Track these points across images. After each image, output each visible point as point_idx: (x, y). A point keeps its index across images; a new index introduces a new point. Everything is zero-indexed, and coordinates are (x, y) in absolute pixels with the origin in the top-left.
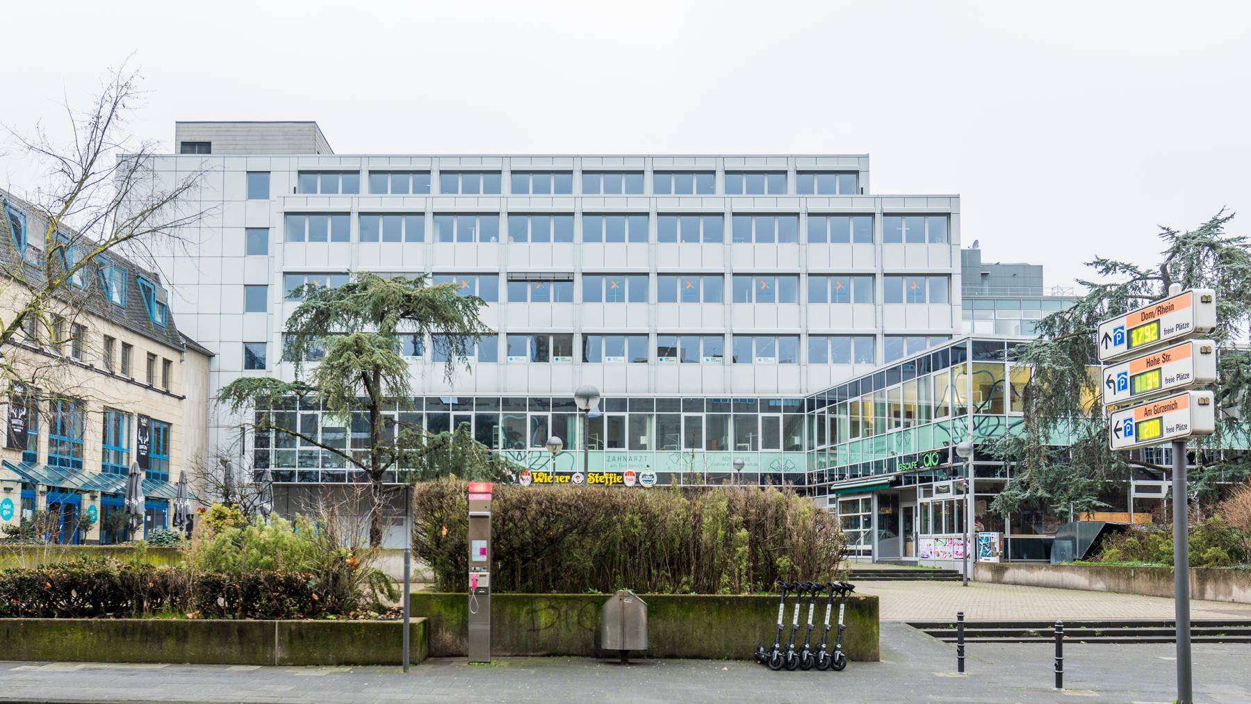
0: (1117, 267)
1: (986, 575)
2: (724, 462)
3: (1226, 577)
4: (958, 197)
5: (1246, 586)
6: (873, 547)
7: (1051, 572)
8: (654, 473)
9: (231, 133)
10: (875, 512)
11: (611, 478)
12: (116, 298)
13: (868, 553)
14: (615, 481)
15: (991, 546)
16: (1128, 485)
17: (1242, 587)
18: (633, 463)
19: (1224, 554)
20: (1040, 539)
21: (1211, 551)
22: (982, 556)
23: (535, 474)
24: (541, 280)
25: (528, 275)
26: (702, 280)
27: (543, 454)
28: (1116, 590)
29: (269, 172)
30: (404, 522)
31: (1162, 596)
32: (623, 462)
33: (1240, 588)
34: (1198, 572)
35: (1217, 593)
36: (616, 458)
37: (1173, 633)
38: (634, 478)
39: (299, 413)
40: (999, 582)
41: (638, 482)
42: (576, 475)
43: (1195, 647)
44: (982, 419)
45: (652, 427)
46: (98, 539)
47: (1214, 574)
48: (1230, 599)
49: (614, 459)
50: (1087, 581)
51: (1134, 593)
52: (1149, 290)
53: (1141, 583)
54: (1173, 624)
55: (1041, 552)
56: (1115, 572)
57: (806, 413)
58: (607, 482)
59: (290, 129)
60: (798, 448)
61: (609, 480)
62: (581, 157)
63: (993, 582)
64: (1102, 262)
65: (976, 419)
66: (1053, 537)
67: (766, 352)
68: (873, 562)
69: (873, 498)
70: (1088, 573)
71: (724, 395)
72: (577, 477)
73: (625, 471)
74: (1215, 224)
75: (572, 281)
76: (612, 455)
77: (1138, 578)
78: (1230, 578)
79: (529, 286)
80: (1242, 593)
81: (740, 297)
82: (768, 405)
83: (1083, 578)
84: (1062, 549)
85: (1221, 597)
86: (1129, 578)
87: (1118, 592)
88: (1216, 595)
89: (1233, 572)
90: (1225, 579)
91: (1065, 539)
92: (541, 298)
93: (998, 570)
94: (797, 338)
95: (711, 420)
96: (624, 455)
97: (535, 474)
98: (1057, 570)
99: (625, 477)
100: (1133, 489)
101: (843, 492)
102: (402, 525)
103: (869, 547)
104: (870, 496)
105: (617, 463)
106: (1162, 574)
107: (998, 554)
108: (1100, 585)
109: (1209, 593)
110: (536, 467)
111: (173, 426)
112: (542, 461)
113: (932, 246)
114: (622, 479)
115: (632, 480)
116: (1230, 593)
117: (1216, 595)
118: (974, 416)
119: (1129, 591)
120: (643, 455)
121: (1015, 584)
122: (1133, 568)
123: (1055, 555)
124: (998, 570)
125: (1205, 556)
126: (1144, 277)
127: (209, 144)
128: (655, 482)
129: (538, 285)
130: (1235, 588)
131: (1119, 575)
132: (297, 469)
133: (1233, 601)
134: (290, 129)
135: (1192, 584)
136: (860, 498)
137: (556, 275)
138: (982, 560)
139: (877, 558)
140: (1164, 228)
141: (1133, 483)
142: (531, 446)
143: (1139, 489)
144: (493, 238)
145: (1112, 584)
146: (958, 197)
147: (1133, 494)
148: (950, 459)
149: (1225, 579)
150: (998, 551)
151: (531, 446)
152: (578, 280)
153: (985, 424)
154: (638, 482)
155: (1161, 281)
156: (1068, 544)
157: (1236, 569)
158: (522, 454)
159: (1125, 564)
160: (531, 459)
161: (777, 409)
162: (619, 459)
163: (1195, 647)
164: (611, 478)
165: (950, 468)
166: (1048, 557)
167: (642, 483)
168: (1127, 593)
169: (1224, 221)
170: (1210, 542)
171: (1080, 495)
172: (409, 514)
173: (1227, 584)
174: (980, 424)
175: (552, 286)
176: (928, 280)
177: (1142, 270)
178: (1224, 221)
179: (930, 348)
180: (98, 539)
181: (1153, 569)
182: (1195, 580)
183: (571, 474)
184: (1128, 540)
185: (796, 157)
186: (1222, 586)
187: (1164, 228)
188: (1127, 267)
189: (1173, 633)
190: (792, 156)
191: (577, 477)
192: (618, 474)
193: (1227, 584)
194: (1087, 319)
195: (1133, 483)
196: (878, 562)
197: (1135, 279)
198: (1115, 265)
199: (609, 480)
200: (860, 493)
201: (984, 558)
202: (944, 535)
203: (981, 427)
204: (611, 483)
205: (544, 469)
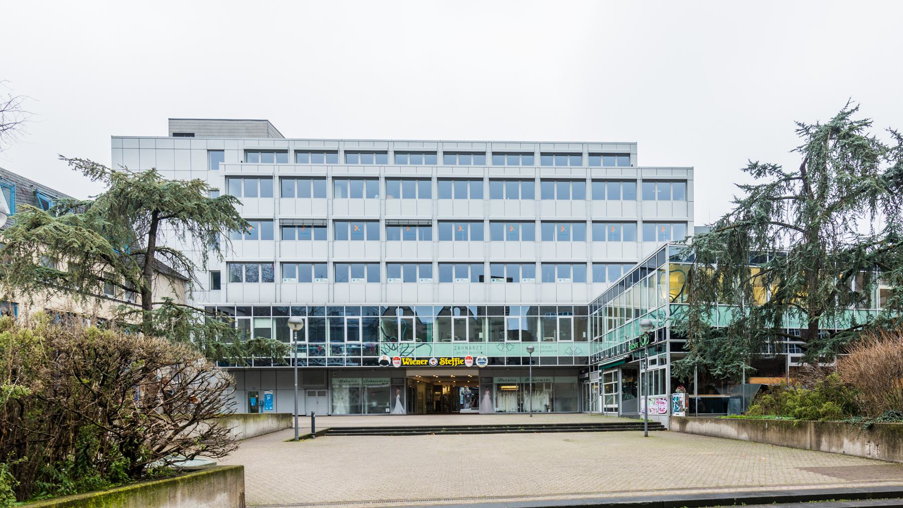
0: (767, 170)
1: (676, 426)
3: (838, 430)
4: (692, 169)
5: (855, 439)
6: (619, 406)
7: (713, 424)
8: (486, 357)
9: (208, 127)
10: (620, 381)
11: (456, 361)
13: (616, 410)
15: (679, 403)
16: (784, 359)
17: (852, 440)
18: (472, 350)
19: (838, 409)
20: (721, 398)
21: (827, 406)
22: (675, 411)
23: (403, 359)
24: (409, 225)
25: (400, 221)
26: (520, 225)
27: (410, 345)
28: (756, 440)
29: (223, 150)
30: (326, 394)
31: (787, 446)
32: (465, 350)
33: (851, 440)
34: (816, 425)
35: (830, 444)
36: (472, 348)
38: (472, 361)
40: (682, 431)
41: (474, 364)
42: (432, 359)
44: (676, 307)
45: (486, 327)
47: (829, 428)
48: (841, 451)
50: (736, 432)
51: (768, 443)
52: (792, 189)
53: (772, 435)
55: (718, 408)
56: (756, 425)
57: (589, 316)
58: (453, 364)
59: (250, 125)
60: (585, 340)
61: (455, 362)
62: (443, 142)
63: (679, 432)
64: (755, 166)
65: (672, 307)
66: (729, 397)
67: (564, 275)
68: (619, 416)
69: (618, 371)
70: (737, 426)
72: (433, 361)
73: (466, 357)
74: (843, 116)
75: (431, 226)
77: (770, 430)
78: (841, 431)
79: (402, 229)
80: (852, 446)
81: (547, 237)
82: (565, 310)
83: (733, 429)
84: (734, 406)
85: (834, 449)
86: (764, 430)
87: (756, 442)
88: (830, 447)
89: (845, 426)
90: (837, 432)
91: (737, 397)
92: (410, 237)
93: (683, 422)
96: (466, 345)
97: (403, 359)
98: (717, 423)
99: (466, 361)
100: (789, 359)
101: (606, 367)
102: (325, 395)
103: (616, 406)
104: (616, 370)
106: (788, 427)
107: (684, 410)
108: (744, 436)
109: (824, 446)
110: (405, 354)
112: (409, 350)
113: (675, 202)
114: (464, 361)
115: (470, 362)
116: (841, 446)
117: (830, 447)
118: (670, 305)
119: (765, 442)
120: (482, 345)
121: (692, 433)
122: (767, 421)
123: (730, 409)
124: (683, 422)
125: (821, 411)
126: (788, 178)
127: (194, 134)
128: (486, 364)
129: (408, 229)
130: (846, 441)
131: (757, 427)
132: (362, 357)
133: (844, 453)
134: (250, 125)
135: (811, 436)
136: (613, 371)
137: (420, 221)
138: (675, 414)
139: (621, 414)
140: (799, 124)
141: (790, 355)
142: (402, 340)
143: (794, 360)
144: (376, 196)
145: (753, 434)
146: (692, 169)
147: (790, 364)
148: (656, 339)
149: (837, 432)
150: (684, 407)
151: (402, 340)
152: (435, 224)
153: (679, 311)
154: (474, 364)
155: (801, 181)
156: (738, 401)
157: (847, 423)
158: (396, 345)
159: (764, 418)
160: (401, 349)
164: (456, 361)
165: (656, 345)
166: (726, 411)
167: (478, 364)
168: (763, 443)
169: (849, 113)
170: (827, 397)
171: (732, 361)
172: (329, 388)
173: (839, 437)
174: (675, 311)
175: (417, 229)
176: (673, 226)
177: (788, 172)
178: (849, 113)
181: (782, 422)
182: (813, 433)
183: (428, 359)
184: (764, 397)
185: (588, 143)
186: (834, 439)
187: (799, 124)
188: (774, 168)
190: (585, 143)
191: (433, 361)
192: (461, 358)
193: (839, 437)
194: (744, 217)
195: (790, 355)
196: (623, 416)
197: (780, 181)
198: (764, 168)
199: (455, 362)
200: (344, 369)
201: (676, 413)
202: (654, 396)
203: (676, 313)
204: (456, 364)
205: (410, 356)
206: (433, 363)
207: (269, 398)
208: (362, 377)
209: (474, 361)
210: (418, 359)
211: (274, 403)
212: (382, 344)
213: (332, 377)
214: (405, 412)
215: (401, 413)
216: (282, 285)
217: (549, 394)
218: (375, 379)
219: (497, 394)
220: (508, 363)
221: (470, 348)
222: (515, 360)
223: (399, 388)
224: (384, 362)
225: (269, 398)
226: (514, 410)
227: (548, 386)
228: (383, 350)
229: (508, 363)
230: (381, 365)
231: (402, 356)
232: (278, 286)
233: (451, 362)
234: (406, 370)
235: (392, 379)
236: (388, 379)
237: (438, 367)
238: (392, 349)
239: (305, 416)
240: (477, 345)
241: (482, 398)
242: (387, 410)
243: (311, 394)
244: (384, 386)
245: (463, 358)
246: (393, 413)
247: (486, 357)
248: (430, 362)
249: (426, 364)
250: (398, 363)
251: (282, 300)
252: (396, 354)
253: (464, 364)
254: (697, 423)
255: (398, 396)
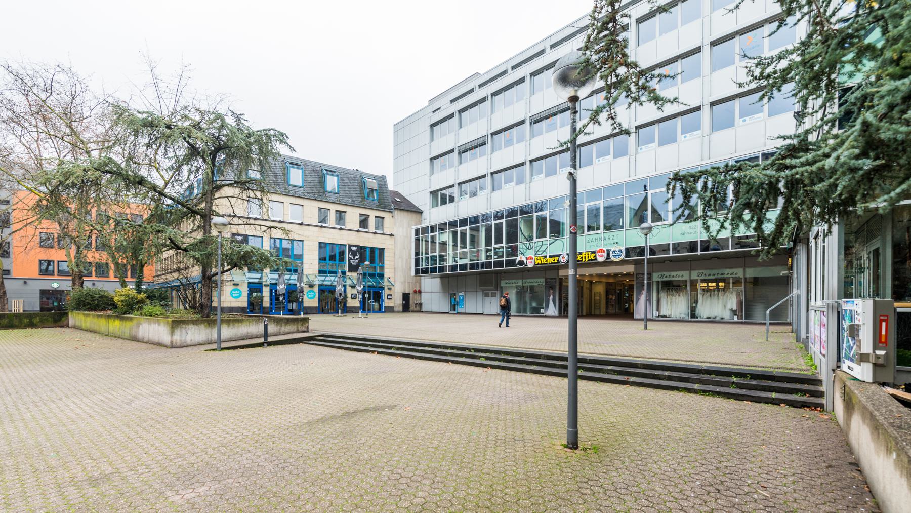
2: (691, 231)
8: (621, 248)
11: (587, 256)
12: (375, 198)
14: (590, 258)
27: (544, 243)
36: (594, 239)
37: (565, 367)
39: (535, 215)
42: (562, 256)
43: (581, 384)
46: (316, 305)
49: (592, 241)
54: (564, 359)
58: (584, 260)
71: (525, 202)
76: (590, 237)
94: (301, 242)
95: (509, 224)
99: (597, 254)
105: (594, 243)
111: (385, 251)
112: (543, 248)
114: (595, 256)
132: (504, 259)
133: (134, 339)
147: (424, 267)
151: (537, 238)
158: (531, 244)
161: (502, 217)
162: (596, 239)
163: (581, 384)
164: (587, 256)
179: (418, 210)
180: (316, 305)
183: (559, 256)
189: (565, 367)
191: (563, 257)
200: (671, 260)
204: (587, 260)
206: (601, 258)
207: (461, 298)
208: (523, 278)
209: (608, 255)
210: (551, 257)
211: (464, 303)
212: (521, 245)
213: (501, 279)
214: (556, 314)
215: (553, 314)
216: (531, 184)
217: (738, 295)
218: (510, 281)
219: (658, 292)
220: (471, 269)
221: (605, 239)
222: (692, 246)
223: (552, 289)
224: (521, 263)
225: (461, 298)
226: (683, 316)
227: (737, 282)
228: (521, 250)
229: (471, 269)
230: (518, 266)
231: (537, 255)
232: (633, 159)
233: (582, 258)
234: (558, 270)
235: (546, 279)
236: (543, 280)
237: (608, 263)
238: (528, 249)
239: (482, 314)
240: (614, 234)
241: (638, 300)
242: (542, 311)
243: (487, 295)
244: (673, 279)
245: (594, 252)
246: (546, 314)
247: (623, 249)
248: (561, 259)
249: (556, 261)
250: (531, 262)
251: (492, 207)
252: (531, 253)
253: (596, 259)
254: (117, 323)
255: (551, 297)
